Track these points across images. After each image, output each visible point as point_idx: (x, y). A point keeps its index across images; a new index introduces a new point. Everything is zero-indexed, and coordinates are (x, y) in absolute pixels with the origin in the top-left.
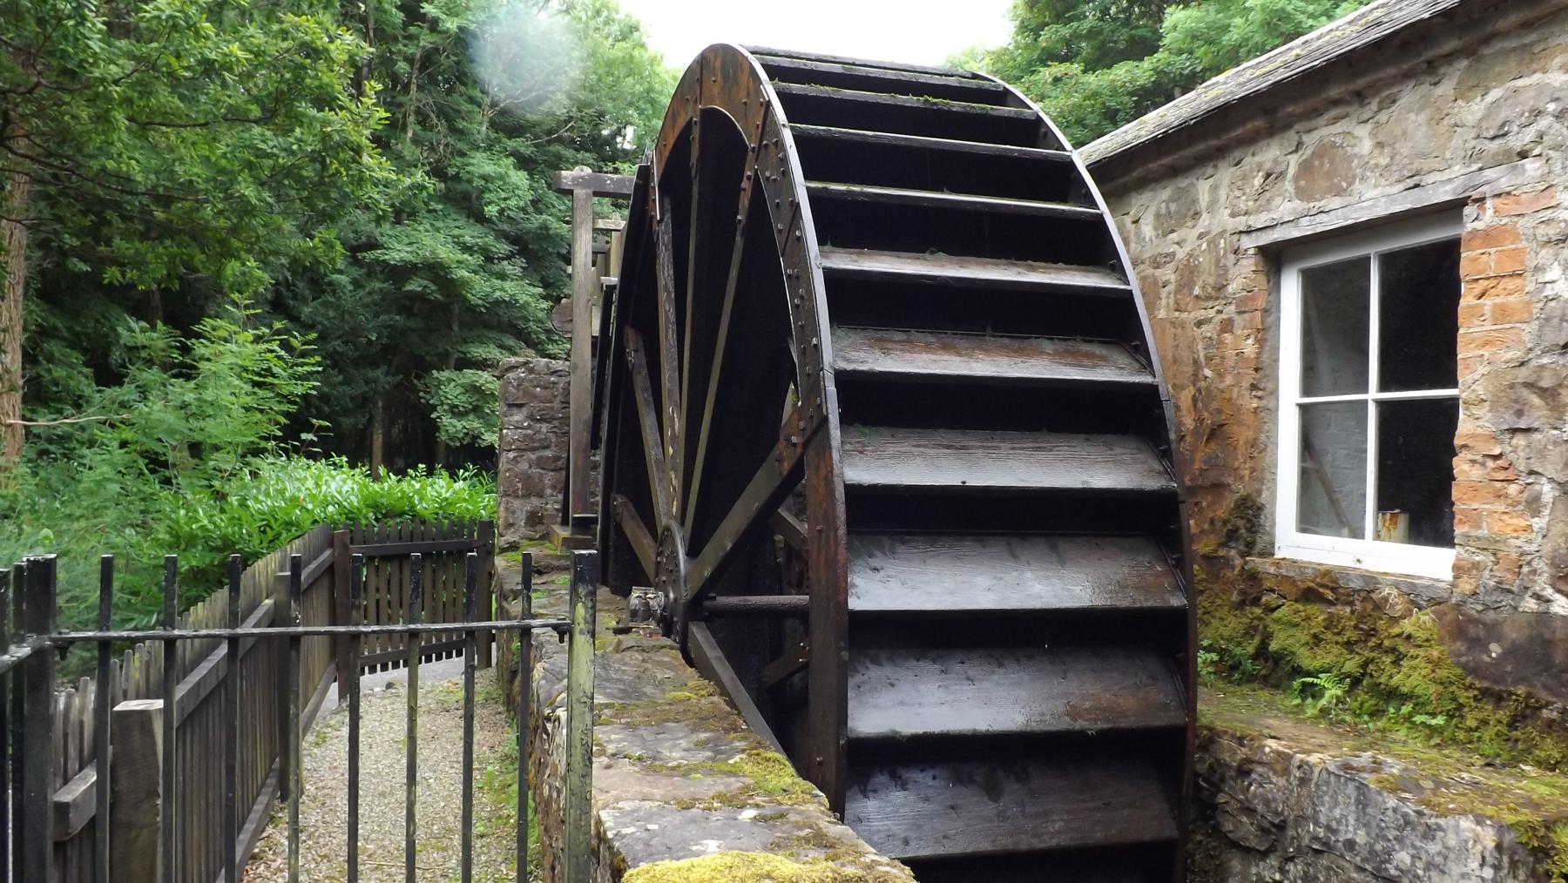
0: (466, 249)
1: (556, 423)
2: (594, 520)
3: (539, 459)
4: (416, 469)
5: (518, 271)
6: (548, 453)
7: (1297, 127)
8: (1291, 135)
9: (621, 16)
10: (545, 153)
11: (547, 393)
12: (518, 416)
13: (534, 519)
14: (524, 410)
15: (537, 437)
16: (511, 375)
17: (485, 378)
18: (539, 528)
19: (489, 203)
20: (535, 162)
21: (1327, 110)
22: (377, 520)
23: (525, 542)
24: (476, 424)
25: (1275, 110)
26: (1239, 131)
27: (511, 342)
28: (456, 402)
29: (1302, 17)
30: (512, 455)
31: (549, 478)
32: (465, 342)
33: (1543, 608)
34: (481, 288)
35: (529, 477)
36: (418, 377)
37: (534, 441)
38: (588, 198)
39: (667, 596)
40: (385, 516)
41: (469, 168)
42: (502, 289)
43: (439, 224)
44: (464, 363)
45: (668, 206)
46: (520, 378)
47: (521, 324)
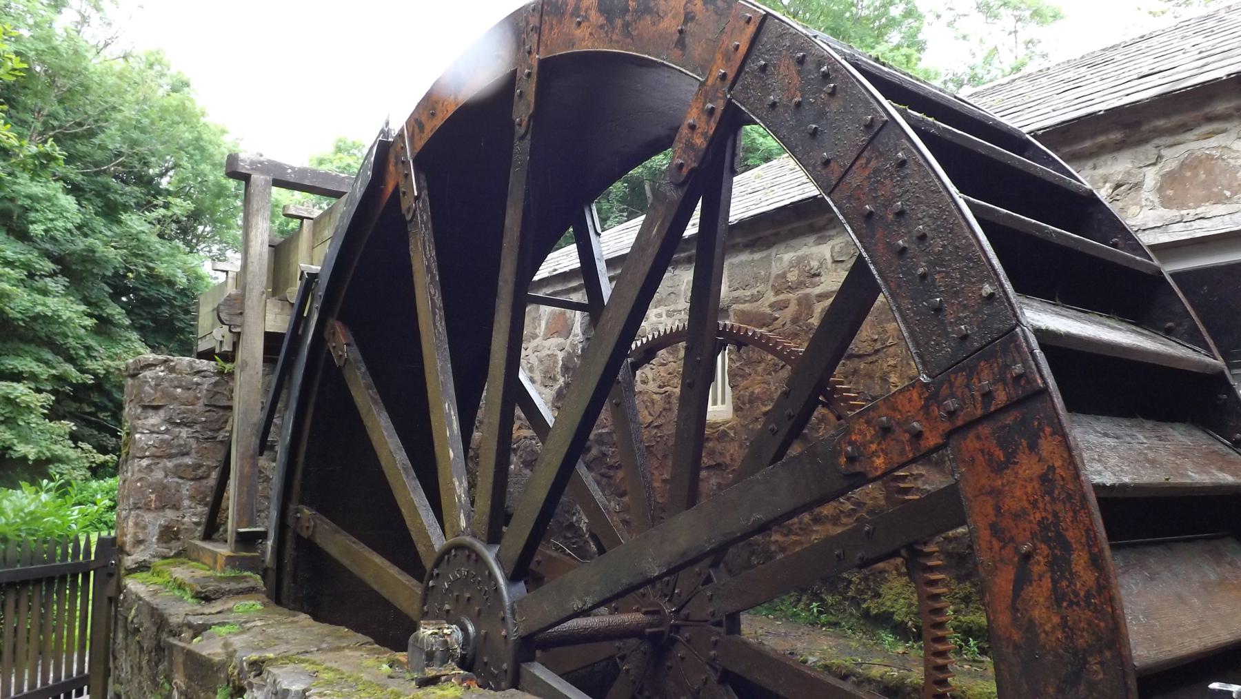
1: (198, 427)
2: (264, 535)
3: (177, 466)
5: (60, 288)
6: (188, 460)
7: (1156, 142)
8: (1150, 149)
9: (173, 71)
10: (93, 182)
12: (154, 419)
13: (168, 534)
14: (162, 413)
15: (175, 442)
16: (148, 373)
17: (20, 390)
18: (174, 544)
19: (33, 223)
21: (1199, 125)
23: (158, 561)
25: (1139, 124)
26: (1088, 144)
27: (49, 356)
29: (756, 135)
30: (145, 462)
31: (187, 488)
33: (1035, 577)
35: (165, 487)
37: (171, 446)
38: (266, 187)
39: (464, 629)
41: (16, 187)
42: (44, 305)
45: (424, 184)
46: (158, 377)
47: (59, 340)
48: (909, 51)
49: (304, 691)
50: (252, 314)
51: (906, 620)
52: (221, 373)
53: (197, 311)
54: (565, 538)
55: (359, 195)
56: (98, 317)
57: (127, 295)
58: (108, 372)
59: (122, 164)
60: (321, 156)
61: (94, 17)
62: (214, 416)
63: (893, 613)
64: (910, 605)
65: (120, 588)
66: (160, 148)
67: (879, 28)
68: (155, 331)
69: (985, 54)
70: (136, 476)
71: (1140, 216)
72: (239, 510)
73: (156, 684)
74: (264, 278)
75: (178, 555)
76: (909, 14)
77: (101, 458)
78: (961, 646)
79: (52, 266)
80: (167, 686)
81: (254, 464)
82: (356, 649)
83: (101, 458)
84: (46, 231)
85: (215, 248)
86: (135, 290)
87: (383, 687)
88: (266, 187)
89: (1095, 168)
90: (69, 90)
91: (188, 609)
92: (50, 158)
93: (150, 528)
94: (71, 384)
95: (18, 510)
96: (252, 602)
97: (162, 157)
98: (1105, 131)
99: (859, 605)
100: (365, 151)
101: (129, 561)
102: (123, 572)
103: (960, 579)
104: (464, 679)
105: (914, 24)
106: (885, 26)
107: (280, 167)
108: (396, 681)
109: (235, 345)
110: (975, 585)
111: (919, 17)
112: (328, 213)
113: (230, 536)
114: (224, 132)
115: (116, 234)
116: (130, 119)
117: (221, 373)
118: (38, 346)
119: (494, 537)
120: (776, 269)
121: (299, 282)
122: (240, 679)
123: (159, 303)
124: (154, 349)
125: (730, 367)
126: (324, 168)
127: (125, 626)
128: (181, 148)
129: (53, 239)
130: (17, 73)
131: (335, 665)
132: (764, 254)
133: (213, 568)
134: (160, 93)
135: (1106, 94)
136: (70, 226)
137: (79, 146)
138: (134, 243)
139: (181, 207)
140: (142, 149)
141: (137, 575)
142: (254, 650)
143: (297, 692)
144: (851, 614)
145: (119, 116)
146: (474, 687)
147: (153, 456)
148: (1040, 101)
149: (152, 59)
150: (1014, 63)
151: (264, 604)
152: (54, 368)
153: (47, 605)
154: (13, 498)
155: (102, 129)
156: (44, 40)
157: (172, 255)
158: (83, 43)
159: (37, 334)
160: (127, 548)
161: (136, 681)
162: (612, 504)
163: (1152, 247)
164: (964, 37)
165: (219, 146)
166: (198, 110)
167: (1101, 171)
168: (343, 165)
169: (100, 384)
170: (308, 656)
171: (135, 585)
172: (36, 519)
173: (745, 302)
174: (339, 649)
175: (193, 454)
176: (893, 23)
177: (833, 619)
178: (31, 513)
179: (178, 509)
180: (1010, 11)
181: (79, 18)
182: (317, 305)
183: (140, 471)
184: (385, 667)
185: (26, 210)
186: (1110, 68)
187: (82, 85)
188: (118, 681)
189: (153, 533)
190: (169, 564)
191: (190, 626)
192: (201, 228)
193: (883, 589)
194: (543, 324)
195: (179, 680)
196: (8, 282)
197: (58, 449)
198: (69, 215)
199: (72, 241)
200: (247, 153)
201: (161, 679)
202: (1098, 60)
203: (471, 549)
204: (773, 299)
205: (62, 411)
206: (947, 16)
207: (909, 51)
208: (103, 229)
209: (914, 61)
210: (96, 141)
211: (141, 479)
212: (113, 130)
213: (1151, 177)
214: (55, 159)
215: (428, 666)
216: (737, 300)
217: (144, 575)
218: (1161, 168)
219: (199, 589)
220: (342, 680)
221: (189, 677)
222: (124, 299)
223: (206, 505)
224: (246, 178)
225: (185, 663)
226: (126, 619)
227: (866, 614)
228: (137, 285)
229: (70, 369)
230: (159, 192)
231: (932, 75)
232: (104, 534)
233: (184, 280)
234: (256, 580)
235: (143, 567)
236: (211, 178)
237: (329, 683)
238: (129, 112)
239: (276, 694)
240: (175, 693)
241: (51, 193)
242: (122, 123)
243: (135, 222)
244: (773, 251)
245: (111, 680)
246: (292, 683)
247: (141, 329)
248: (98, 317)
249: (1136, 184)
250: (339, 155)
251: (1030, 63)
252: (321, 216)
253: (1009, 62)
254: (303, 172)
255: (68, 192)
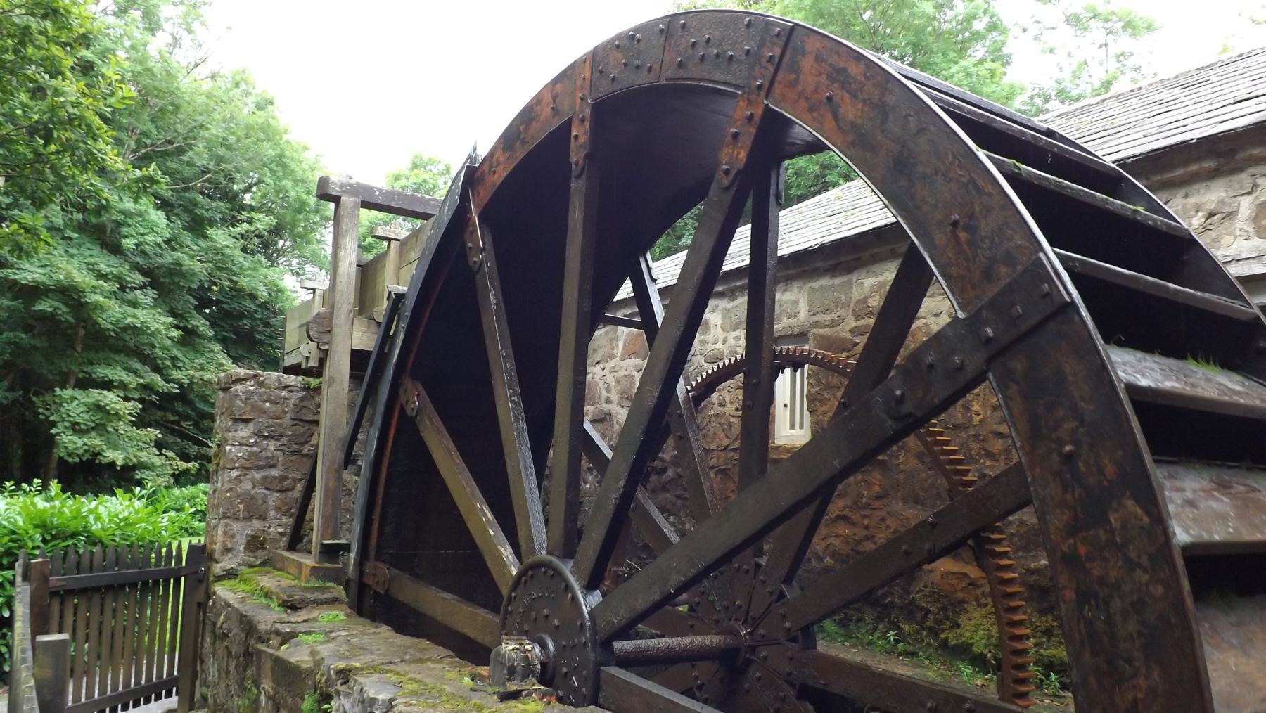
0: (101, 276)
1: (284, 440)
2: (346, 548)
3: (264, 478)
4: (30, 484)
6: (275, 472)
7: (1252, 170)
8: (1245, 178)
9: (258, 90)
10: (181, 198)
11: (277, 408)
12: (244, 432)
13: (255, 543)
14: (251, 425)
15: (264, 454)
17: (110, 398)
18: (260, 553)
19: (126, 237)
20: (171, 205)
22: (44, 541)
23: (246, 570)
24: (98, 442)
25: (1233, 152)
26: (1179, 172)
28: (78, 420)
30: (234, 473)
31: (273, 498)
32: (92, 364)
34: (112, 312)
35: (253, 498)
36: (37, 394)
37: (259, 459)
38: (355, 208)
39: (543, 646)
40: (54, 537)
42: (134, 316)
43: (72, 251)
44: (86, 383)
47: (147, 350)
48: (993, 65)
49: (391, 700)
50: (340, 331)
51: (985, 651)
52: (306, 388)
53: (284, 326)
54: (640, 558)
55: (446, 219)
56: (184, 329)
57: (210, 308)
58: (192, 383)
59: (208, 181)
60: (396, 172)
61: (186, 39)
62: (300, 429)
63: (972, 644)
64: (990, 637)
65: (209, 595)
66: (245, 164)
67: (962, 42)
68: (235, 343)
69: (1074, 67)
70: (227, 486)
71: (1234, 246)
72: (323, 523)
73: (243, 689)
74: (352, 298)
75: (263, 564)
76: (993, 27)
77: (183, 465)
78: (1042, 681)
79: (142, 279)
80: (254, 690)
81: (339, 478)
82: (438, 662)
83: (183, 465)
84: (137, 245)
85: (295, 262)
86: (217, 303)
87: (465, 699)
88: (355, 208)
89: (1187, 196)
90: (161, 110)
91: (275, 617)
92: (152, 180)
93: (238, 537)
94: (157, 393)
95: (113, 517)
96: (335, 612)
97: (246, 174)
98: (1198, 159)
99: (936, 635)
100: (453, 175)
101: (217, 569)
102: (212, 579)
103: (1043, 612)
104: (544, 695)
105: (999, 38)
106: (969, 40)
107: (368, 189)
108: (478, 694)
109: (322, 362)
110: (1056, 619)
111: (1004, 31)
112: (415, 234)
113: (315, 548)
114: (305, 148)
115: (202, 249)
116: (217, 137)
117: (306, 388)
118: (128, 355)
119: (568, 551)
120: (856, 295)
121: (386, 303)
122: (327, 687)
123: (241, 316)
124: (236, 360)
125: (809, 391)
126: (398, 186)
127: (213, 631)
128: (265, 165)
129: (144, 253)
130: (127, 102)
131: (419, 677)
132: (845, 279)
133: (298, 578)
134: (246, 112)
135: (1199, 122)
136: (159, 240)
137: (169, 163)
138: (219, 257)
139: (263, 222)
140: (229, 167)
141: (225, 582)
142: (341, 659)
143: (383, 701)
144: (929, 644)
145: (206, 134)
146: (555, 702)
147: (242, 468)
148: (1131, 125)
149: (238, 78)
150: (1104, 77)
151: (347, 615)
152: (141, 377)
153: (142, 605)
154: (108, 504)
155: (190, 146)
156: (140, 63)
157: (255, 269)
158: (176, 65)
159: (128, 345)
160: (217, 556)
161: (223, 685)
162: (688, 526)
163: (1245, 280)
164: (1051, 51)
165: (300, 162)
166: (281, 127)
167: (1193, 200)
168: (419, 181)
169: (184, 394)
170: (392, 667)
171: (223, 591)
172: (131, 524)
173: (825, 326)
174: (421, 661)
175: (280, 467)
176: (977, 37)
177: (910, 649)
178: (126, 519)
179: (264, 520)
180: (1100, 24)
181: (170, 40)
182: (403, 324)
183: (230, 481)
184: (467, 680)
185: (119, 224)
186: (1205, 89)
187: (172, 104)
188: (205, 684)
189: (241, 542)
190: (255, 573)
191: (278, 633)
192: (281, 242)
193: (963, 620)
194: (621, 344)
195: (267, 685)
196: (102, 294)
197: (144, 457)
198: (158, 230)
199: (161, 255)
200: (338, 174)
201: (249, 684)
202: (1193, 80)
203: (548, 565)
204: (854, 324)
205: (147, 419)
206: (1033, 29)
207: (993, 65)
208: (189, 243)
209: (998, 74)
210: (185, 158)
211: (230, 490)
212: (200, 147)
213: (1246, 206)
214: (157, 182)
215: (509, 680)
216: (816, 325)
217: (232, 582)
218: (1257, 198)
219: (285, 598)
220: (424, 693)
221: (277, 683)
222: (207, 311)
223: (291, 516)
224: (336, 200)
225: (273, 669)
226: (215, 624)
227: (944, 644)
228: (220, 298)
229: (156, 378)
230: (242, 208)
231: (1018, 91)
232: (195, 540)
233: (266, 294)
234: (338, 591)
235: (230, 575)
236: (293, 193)
237: (414, 694)
238: (216, 130)
239: (363, 702)
240: (263, 698)
241: (143, 208)
242: (209, 141)
243: (220, 236)
244: (854, 276)
245: (198, 683)
246: (379, 692)
247: (224, 341)
248: (184, 329)
249: (1230, 214)
250: (416, 171)
251: (1121, 77)
252: (408, 238)
253: (1097, 75)
254: (389, 194)
255: (158, 207)
